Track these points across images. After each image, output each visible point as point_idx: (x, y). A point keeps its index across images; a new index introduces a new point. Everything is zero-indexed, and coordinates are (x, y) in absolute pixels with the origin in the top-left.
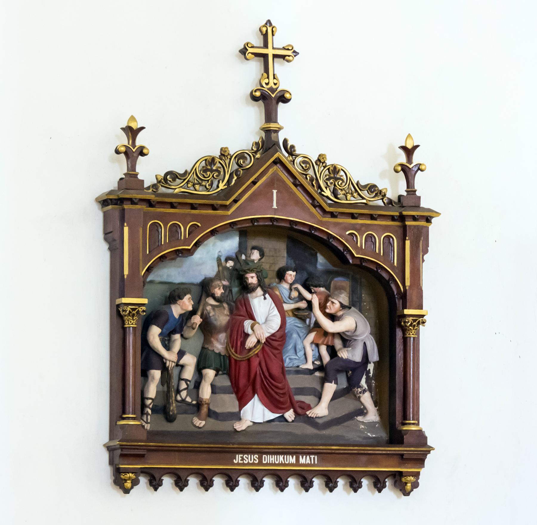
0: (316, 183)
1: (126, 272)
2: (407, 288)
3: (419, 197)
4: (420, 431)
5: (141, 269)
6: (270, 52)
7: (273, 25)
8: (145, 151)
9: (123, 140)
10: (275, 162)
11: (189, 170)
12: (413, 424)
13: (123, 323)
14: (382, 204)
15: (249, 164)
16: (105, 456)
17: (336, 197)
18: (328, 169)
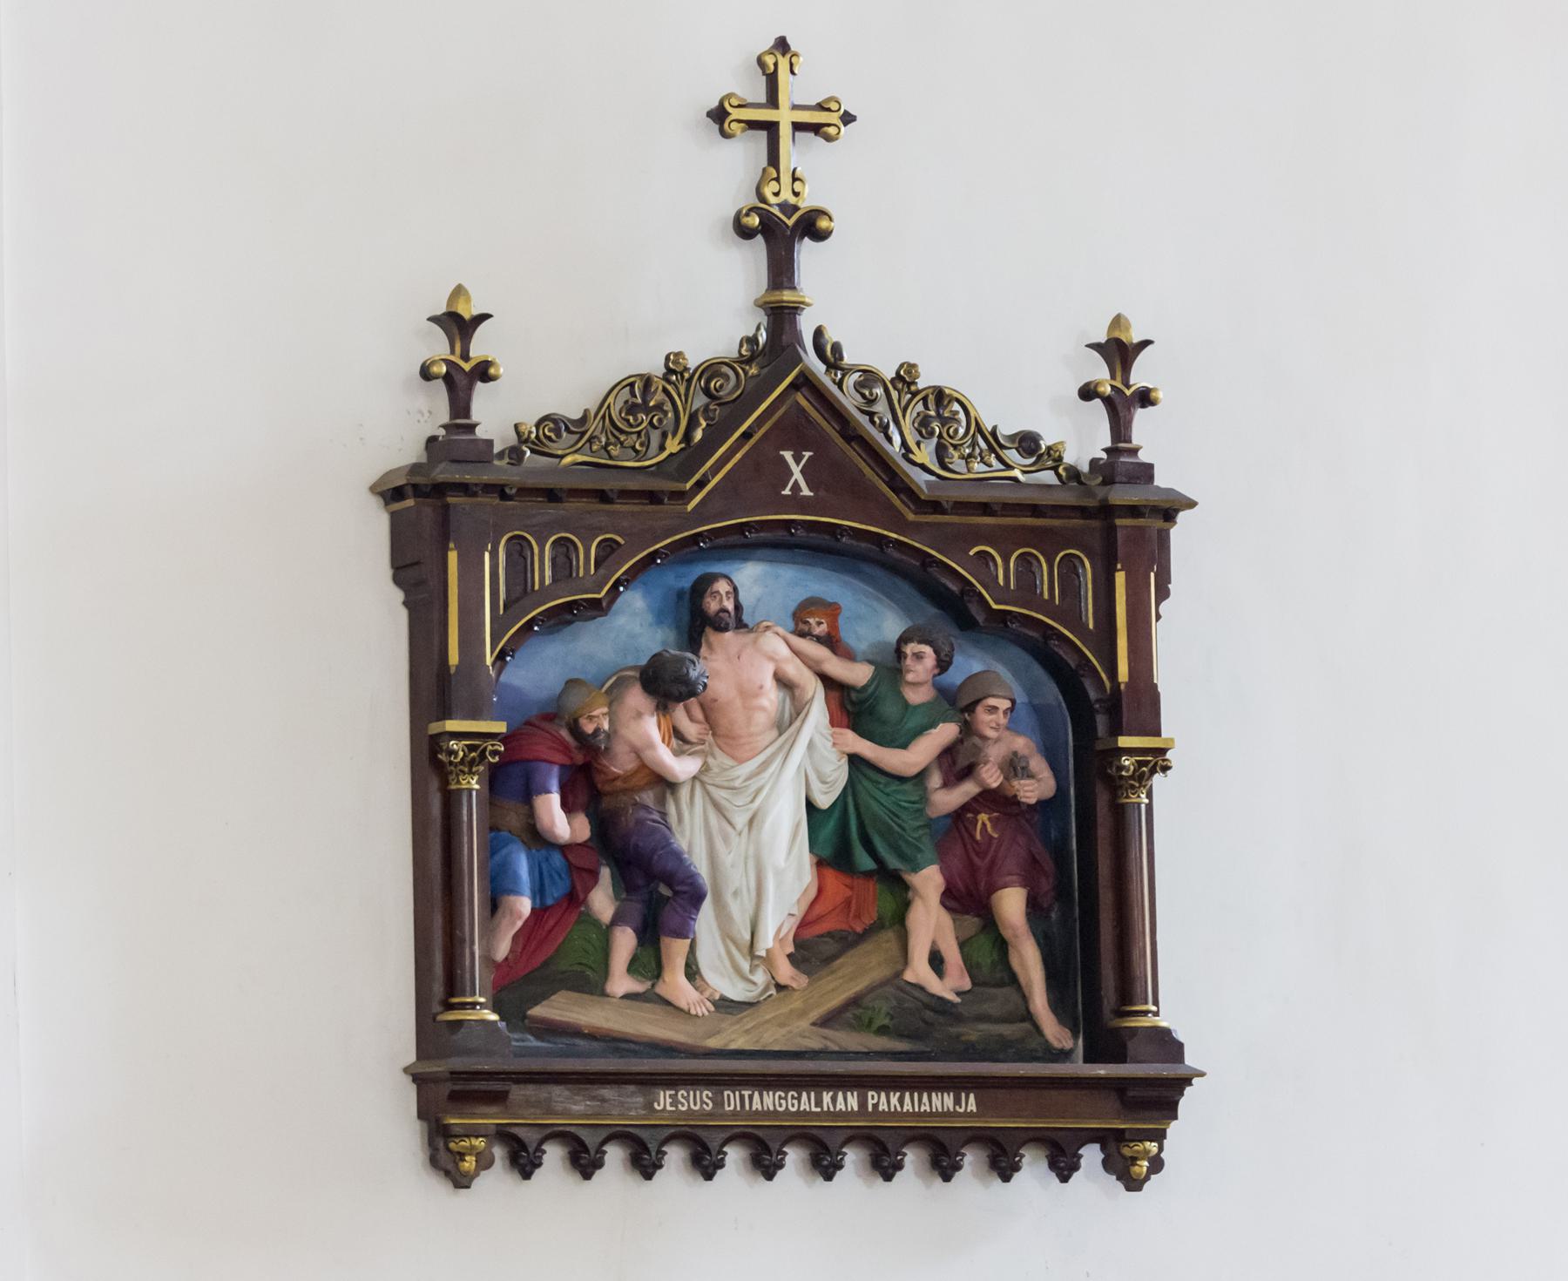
1: (454, 658)
3: (1150, 467)
6: (784, 117)
9: (438, 346)
10: (794, 386)
13: (447, 783)
14: (1057, 482)
15: (728, 388)
16: (408, 1094)
17: (944, 466)
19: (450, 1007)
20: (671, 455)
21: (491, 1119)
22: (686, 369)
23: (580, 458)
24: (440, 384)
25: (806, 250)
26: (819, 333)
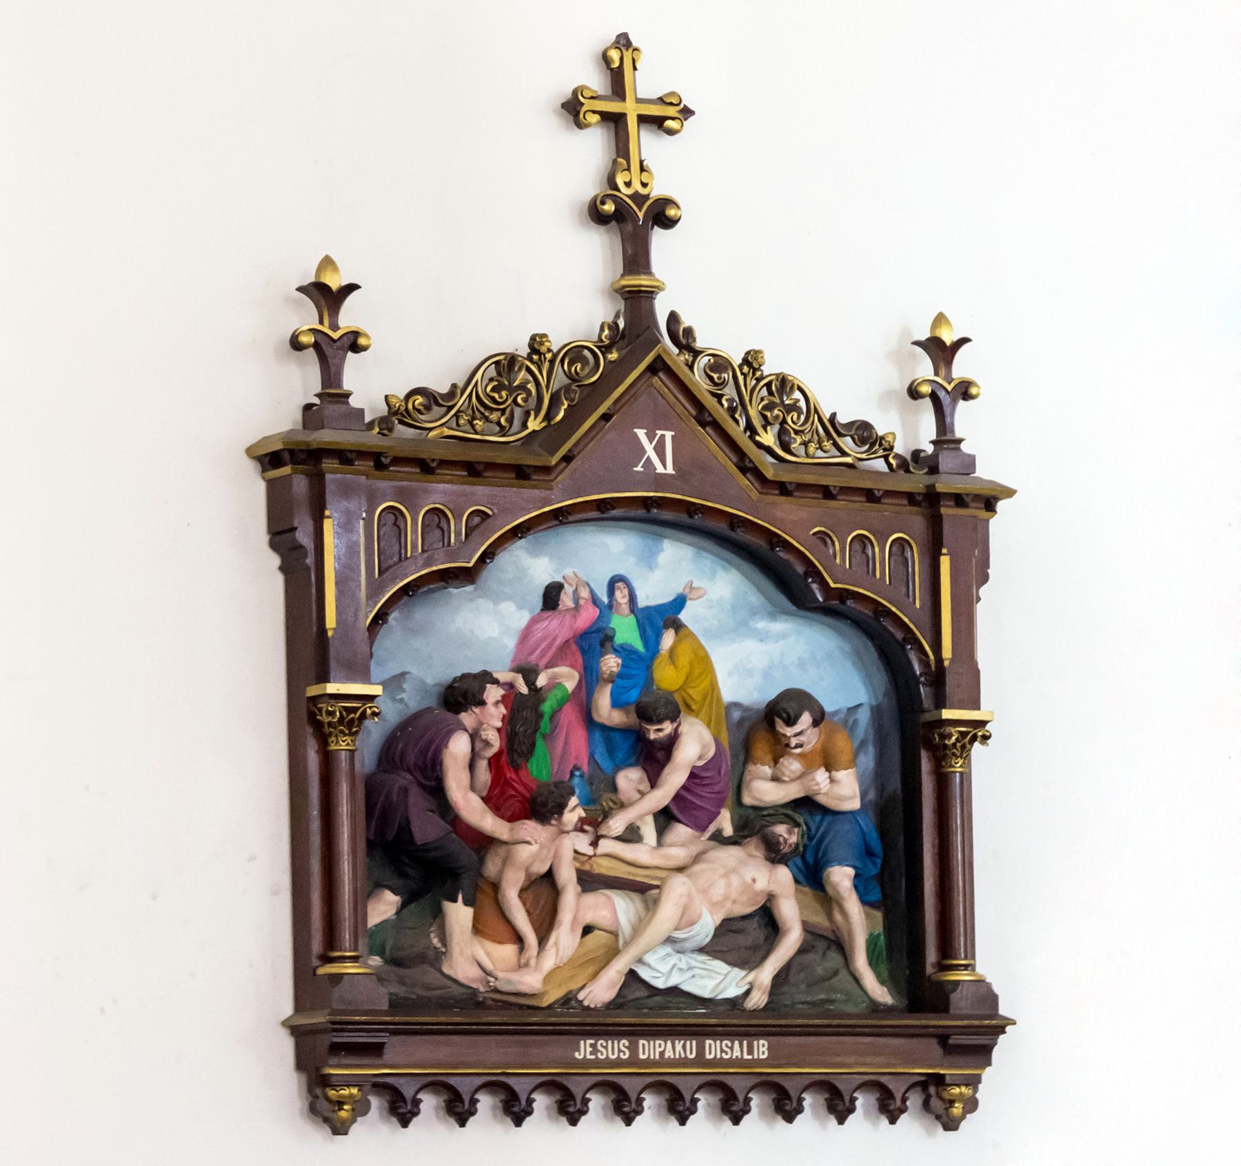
1: (331, 621)
2: (946, 663)
4: (981, 982)
5: (363, 612)
6: (631, 110)
7: (635, 44)
8: (362, 341)
9: (306, 318)
10: (652, 369)
14: (886, 469)
16: (286, 1045)
17: (786, 447)
18: (769, 385)
22: (549, 350)
23: (448, 432)
24: (311, 352)
25: (659, 238)
26: (673, 318)
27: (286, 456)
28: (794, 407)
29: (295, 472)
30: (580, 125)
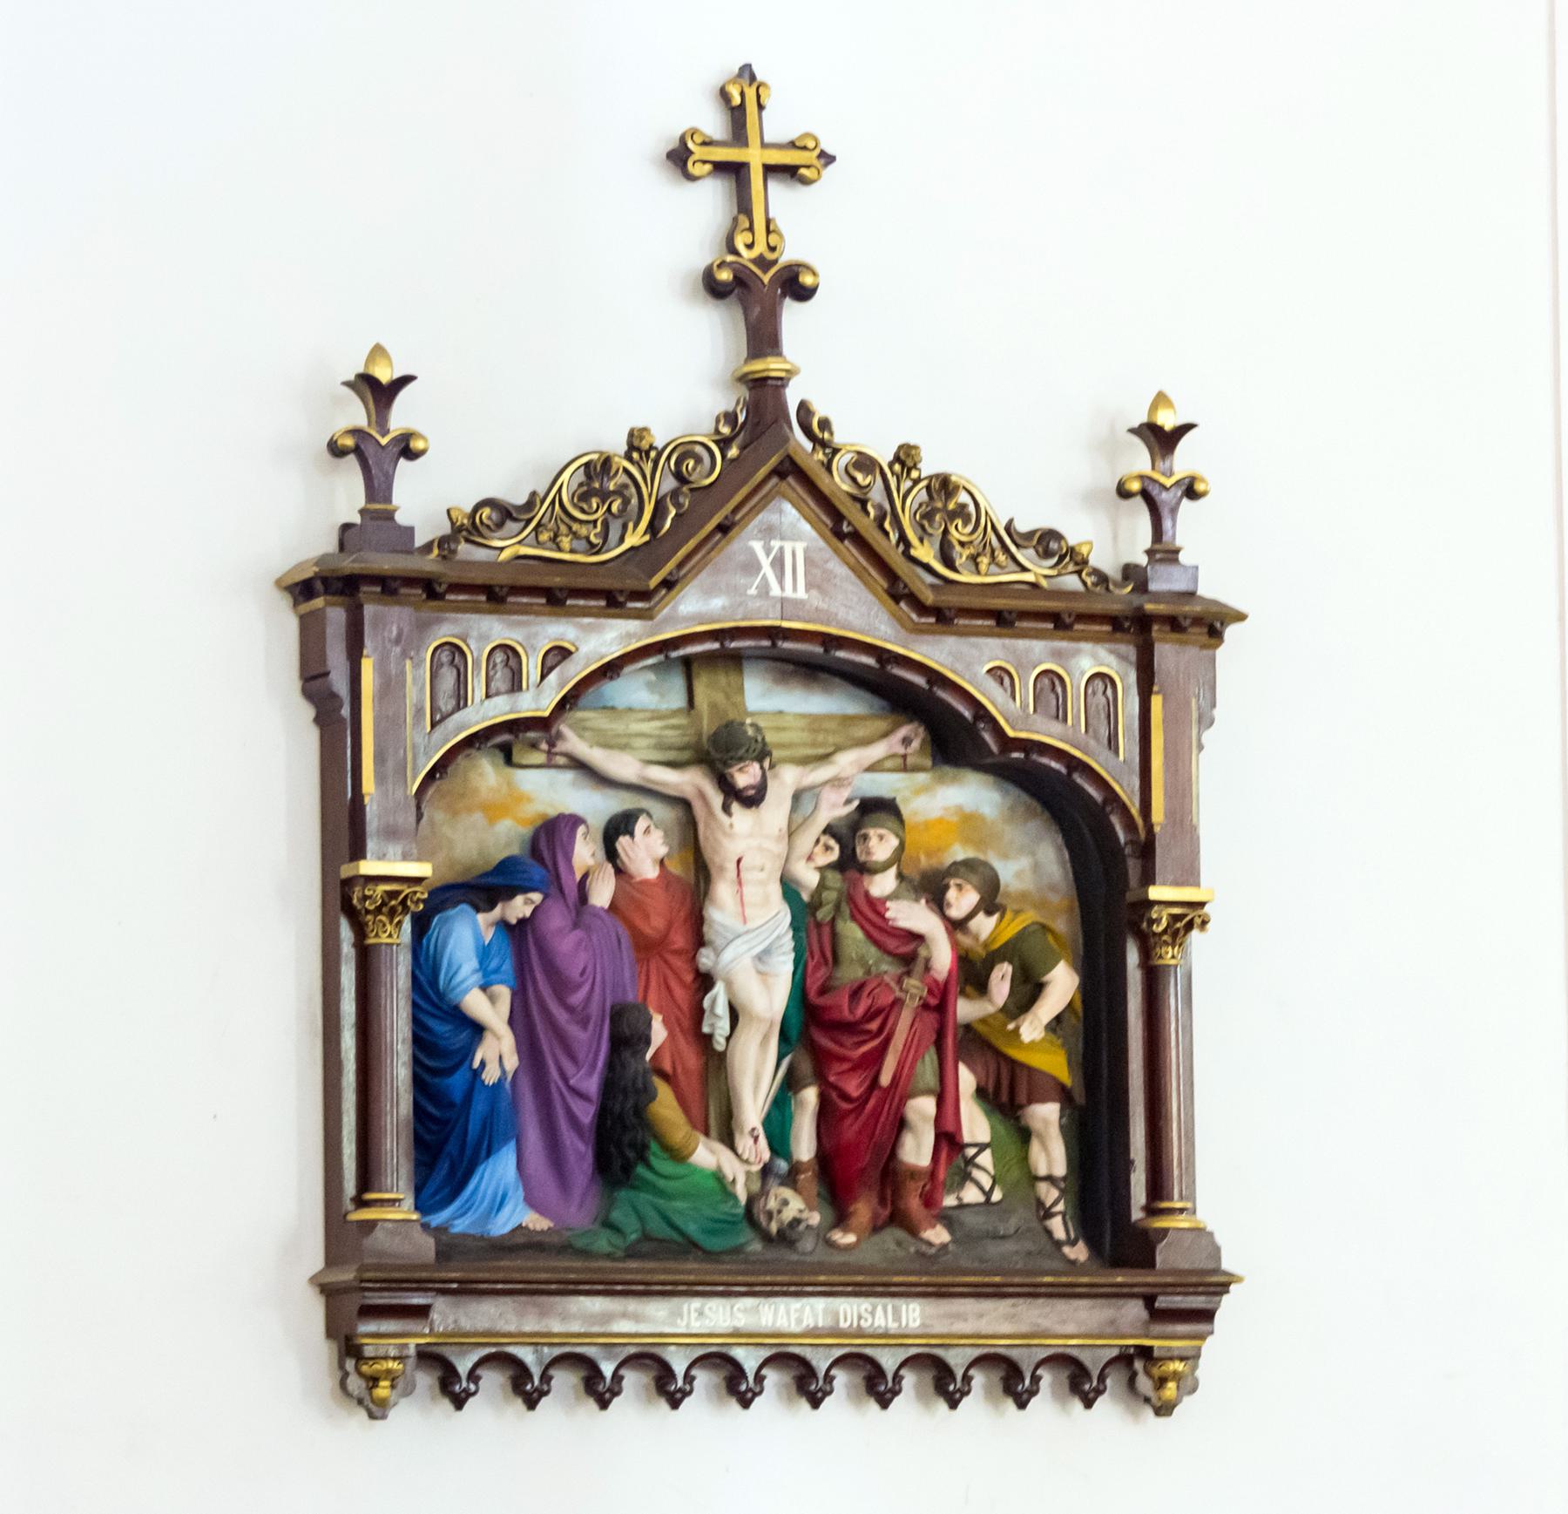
0: (890, 521)
2: (1157, 829)
4: (1199, 1231)
6: (755, 157)
7: (759, 77)
10: (780, 472)
11: (541, 492)
12: (1182, 1210)
14: (1079, 586)
16: (314, 1311)
17: (949, 562)
19: (360, 1203)
20: (632, 548)
21: (416, 1337)
22: (652, 447)
23: (525, 551)
25: (792, 315)
27: (319, 586)
28: (961, 511)
29: (328, 604)
30: (691, 178)
